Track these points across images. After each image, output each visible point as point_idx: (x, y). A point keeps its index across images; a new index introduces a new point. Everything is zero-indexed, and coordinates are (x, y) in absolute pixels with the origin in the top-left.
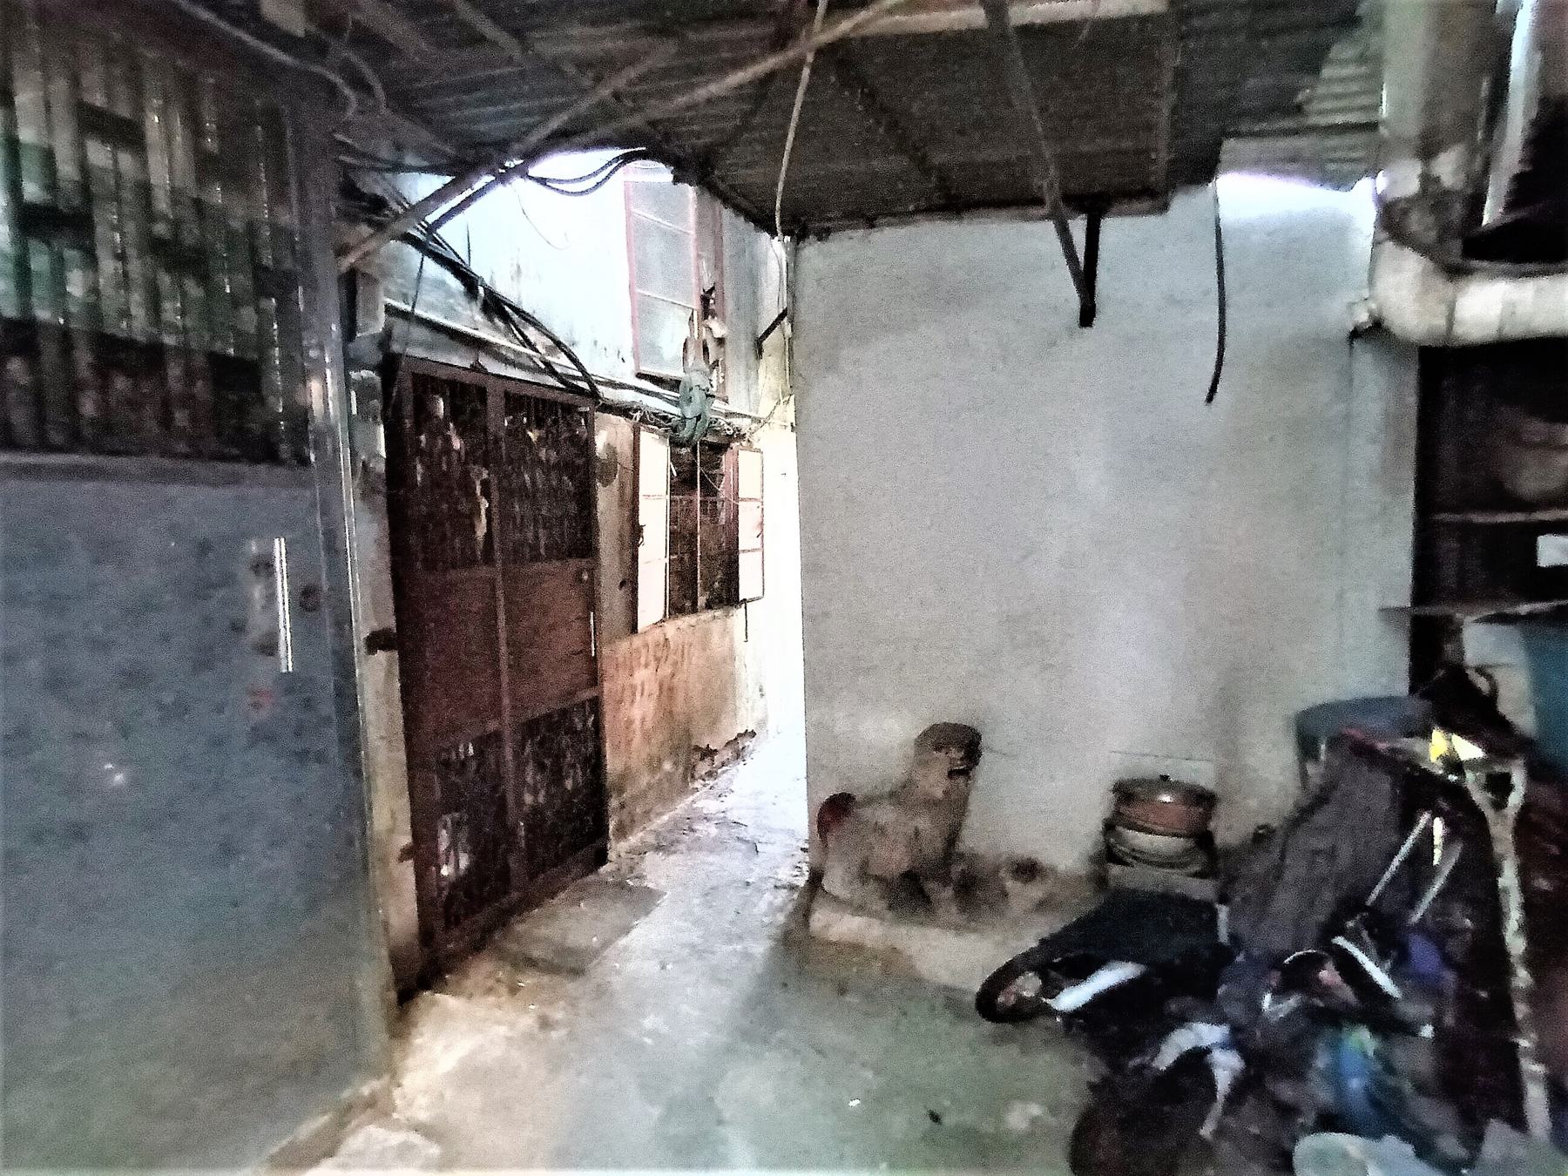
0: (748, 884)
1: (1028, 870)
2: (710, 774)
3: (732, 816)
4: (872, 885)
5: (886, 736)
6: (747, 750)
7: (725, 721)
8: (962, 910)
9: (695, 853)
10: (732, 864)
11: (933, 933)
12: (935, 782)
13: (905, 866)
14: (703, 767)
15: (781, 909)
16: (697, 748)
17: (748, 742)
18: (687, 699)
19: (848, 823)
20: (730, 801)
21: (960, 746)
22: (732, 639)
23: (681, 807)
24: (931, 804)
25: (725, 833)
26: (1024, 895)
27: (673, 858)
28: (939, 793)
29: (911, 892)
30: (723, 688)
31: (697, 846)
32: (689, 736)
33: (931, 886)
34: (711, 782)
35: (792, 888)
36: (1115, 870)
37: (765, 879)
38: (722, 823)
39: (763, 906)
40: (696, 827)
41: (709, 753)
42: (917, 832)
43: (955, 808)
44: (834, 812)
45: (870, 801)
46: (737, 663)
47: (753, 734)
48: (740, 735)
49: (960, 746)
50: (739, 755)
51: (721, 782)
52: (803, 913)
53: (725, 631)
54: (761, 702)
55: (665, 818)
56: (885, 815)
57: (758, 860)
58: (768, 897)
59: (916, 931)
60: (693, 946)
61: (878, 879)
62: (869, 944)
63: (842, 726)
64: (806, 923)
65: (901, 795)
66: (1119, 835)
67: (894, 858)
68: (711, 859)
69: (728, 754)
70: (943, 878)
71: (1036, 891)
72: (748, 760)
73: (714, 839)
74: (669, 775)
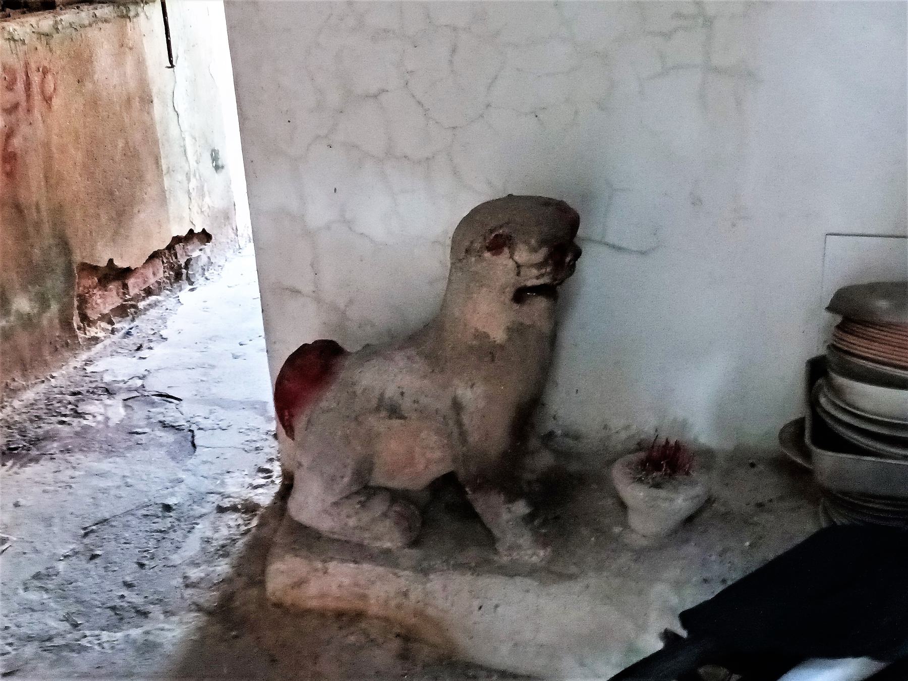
0: (167, 508)
1: (664, 460)
2: (122, 311)
3: (156, 384)
4: (379, 506)
5: (401, 229)
6: (195, 269)
7: (144, 217)
8: (543, 541)
9: (74, 458)
10: (150, 473)
11: (495, 587)
12: (488, 314)
13: (438, 470)
14: (106, 301)
15: (223, 551)
16: (89, 269)
17: (195, 251)
18: (51, 179)
19: (330, 398)
20: (157, 355)
21: (541, 238)
22: (140, 63)
23: (64, 374)
24: (486, 352)
25: (140, 413)
26: (650, 509)
27: (31, 470)
28: (498, 335)
29: (443, 515)
30: (131, 154)
31: (85, 441)
32: (65, 247)
33: (482, 504)
34: (122, 325)
35: (250, 508)
36: (827, 461)
37: (199, 498)
38: (137, 396)
39: (192, 546)
40: (82, 408)
41: (116, 275)
42: (457, 406)
43: (540, 354)
44: (306, 375)
45: (370, 352)
46: (157, 109)
47: (206, 237)
48: (177, 240)
49: (541, 238)
50: (179, 274)
51: (144, 324)
52: (258, 551)
53: (123, 46)
54: (218, 178)
55: (29, 395)
56: (396, 378)
57: (191, 462)
58: (203, 528)
59: (461, 582)
60: (45, 639)
61: (396, 496)
62: (374, 609)
63: (319, 213)
64: (258, 581)
65: (425, 338)
66: (837, 391)
67: (414, 456)
68: (105, 465)
69: (159, 273)
70: (525, 482)
71: (680, 501)
72: (199, 280)
73: (119, 427)
74: (28, 322)
